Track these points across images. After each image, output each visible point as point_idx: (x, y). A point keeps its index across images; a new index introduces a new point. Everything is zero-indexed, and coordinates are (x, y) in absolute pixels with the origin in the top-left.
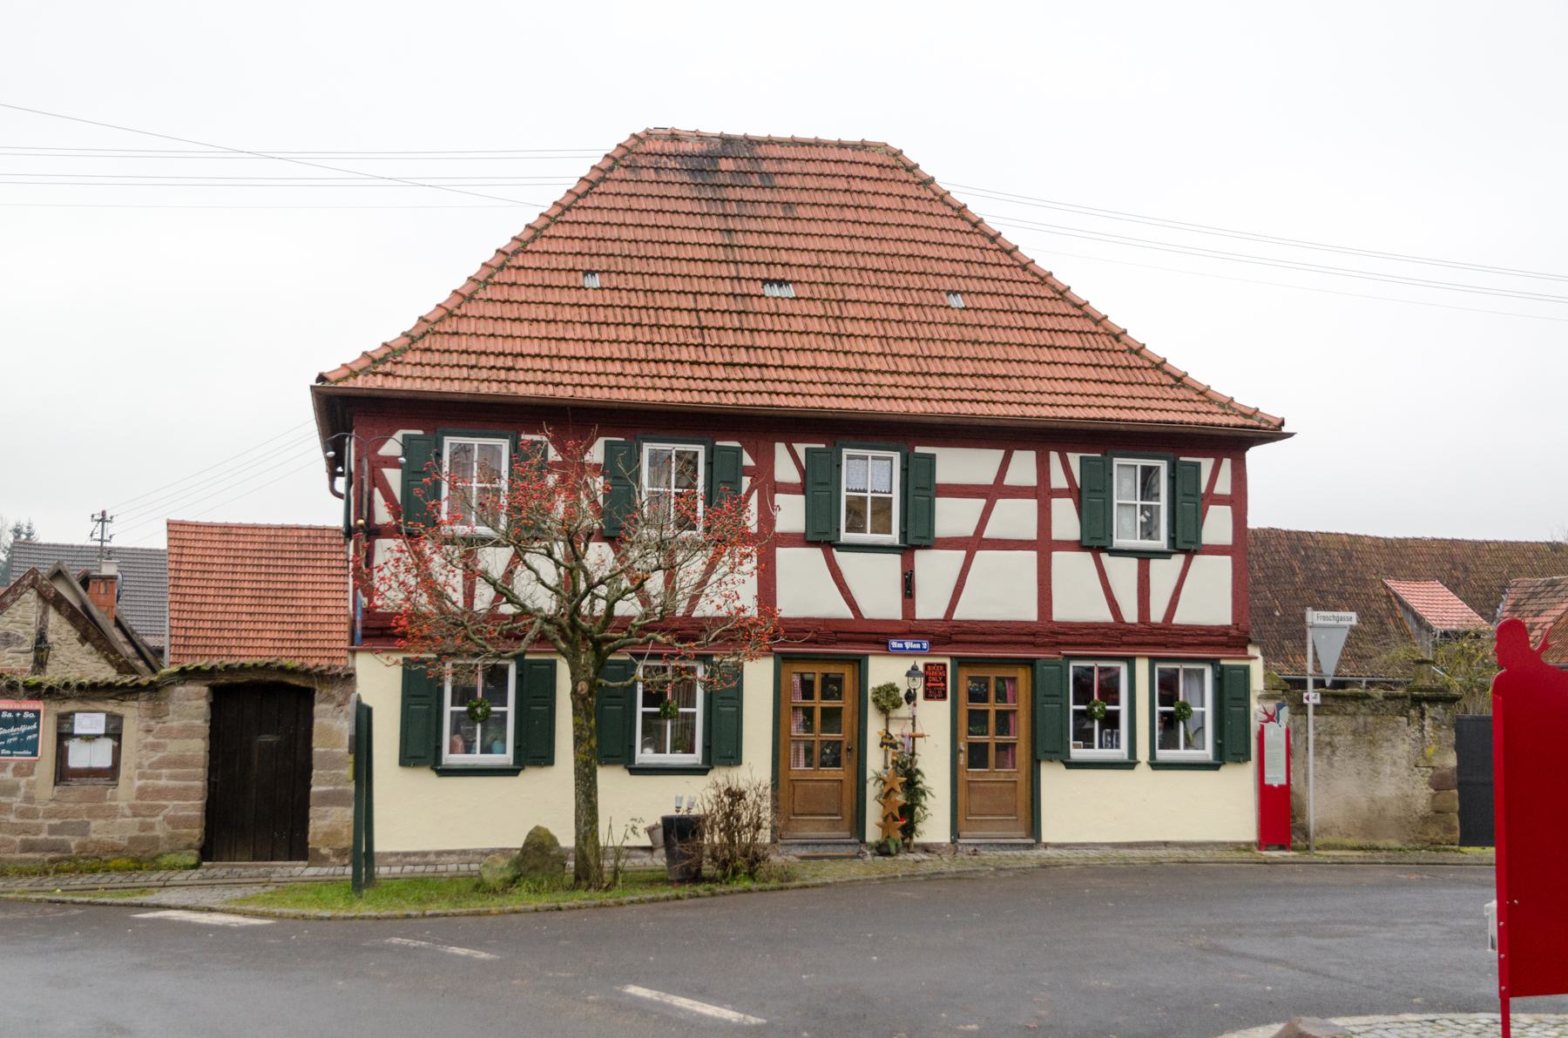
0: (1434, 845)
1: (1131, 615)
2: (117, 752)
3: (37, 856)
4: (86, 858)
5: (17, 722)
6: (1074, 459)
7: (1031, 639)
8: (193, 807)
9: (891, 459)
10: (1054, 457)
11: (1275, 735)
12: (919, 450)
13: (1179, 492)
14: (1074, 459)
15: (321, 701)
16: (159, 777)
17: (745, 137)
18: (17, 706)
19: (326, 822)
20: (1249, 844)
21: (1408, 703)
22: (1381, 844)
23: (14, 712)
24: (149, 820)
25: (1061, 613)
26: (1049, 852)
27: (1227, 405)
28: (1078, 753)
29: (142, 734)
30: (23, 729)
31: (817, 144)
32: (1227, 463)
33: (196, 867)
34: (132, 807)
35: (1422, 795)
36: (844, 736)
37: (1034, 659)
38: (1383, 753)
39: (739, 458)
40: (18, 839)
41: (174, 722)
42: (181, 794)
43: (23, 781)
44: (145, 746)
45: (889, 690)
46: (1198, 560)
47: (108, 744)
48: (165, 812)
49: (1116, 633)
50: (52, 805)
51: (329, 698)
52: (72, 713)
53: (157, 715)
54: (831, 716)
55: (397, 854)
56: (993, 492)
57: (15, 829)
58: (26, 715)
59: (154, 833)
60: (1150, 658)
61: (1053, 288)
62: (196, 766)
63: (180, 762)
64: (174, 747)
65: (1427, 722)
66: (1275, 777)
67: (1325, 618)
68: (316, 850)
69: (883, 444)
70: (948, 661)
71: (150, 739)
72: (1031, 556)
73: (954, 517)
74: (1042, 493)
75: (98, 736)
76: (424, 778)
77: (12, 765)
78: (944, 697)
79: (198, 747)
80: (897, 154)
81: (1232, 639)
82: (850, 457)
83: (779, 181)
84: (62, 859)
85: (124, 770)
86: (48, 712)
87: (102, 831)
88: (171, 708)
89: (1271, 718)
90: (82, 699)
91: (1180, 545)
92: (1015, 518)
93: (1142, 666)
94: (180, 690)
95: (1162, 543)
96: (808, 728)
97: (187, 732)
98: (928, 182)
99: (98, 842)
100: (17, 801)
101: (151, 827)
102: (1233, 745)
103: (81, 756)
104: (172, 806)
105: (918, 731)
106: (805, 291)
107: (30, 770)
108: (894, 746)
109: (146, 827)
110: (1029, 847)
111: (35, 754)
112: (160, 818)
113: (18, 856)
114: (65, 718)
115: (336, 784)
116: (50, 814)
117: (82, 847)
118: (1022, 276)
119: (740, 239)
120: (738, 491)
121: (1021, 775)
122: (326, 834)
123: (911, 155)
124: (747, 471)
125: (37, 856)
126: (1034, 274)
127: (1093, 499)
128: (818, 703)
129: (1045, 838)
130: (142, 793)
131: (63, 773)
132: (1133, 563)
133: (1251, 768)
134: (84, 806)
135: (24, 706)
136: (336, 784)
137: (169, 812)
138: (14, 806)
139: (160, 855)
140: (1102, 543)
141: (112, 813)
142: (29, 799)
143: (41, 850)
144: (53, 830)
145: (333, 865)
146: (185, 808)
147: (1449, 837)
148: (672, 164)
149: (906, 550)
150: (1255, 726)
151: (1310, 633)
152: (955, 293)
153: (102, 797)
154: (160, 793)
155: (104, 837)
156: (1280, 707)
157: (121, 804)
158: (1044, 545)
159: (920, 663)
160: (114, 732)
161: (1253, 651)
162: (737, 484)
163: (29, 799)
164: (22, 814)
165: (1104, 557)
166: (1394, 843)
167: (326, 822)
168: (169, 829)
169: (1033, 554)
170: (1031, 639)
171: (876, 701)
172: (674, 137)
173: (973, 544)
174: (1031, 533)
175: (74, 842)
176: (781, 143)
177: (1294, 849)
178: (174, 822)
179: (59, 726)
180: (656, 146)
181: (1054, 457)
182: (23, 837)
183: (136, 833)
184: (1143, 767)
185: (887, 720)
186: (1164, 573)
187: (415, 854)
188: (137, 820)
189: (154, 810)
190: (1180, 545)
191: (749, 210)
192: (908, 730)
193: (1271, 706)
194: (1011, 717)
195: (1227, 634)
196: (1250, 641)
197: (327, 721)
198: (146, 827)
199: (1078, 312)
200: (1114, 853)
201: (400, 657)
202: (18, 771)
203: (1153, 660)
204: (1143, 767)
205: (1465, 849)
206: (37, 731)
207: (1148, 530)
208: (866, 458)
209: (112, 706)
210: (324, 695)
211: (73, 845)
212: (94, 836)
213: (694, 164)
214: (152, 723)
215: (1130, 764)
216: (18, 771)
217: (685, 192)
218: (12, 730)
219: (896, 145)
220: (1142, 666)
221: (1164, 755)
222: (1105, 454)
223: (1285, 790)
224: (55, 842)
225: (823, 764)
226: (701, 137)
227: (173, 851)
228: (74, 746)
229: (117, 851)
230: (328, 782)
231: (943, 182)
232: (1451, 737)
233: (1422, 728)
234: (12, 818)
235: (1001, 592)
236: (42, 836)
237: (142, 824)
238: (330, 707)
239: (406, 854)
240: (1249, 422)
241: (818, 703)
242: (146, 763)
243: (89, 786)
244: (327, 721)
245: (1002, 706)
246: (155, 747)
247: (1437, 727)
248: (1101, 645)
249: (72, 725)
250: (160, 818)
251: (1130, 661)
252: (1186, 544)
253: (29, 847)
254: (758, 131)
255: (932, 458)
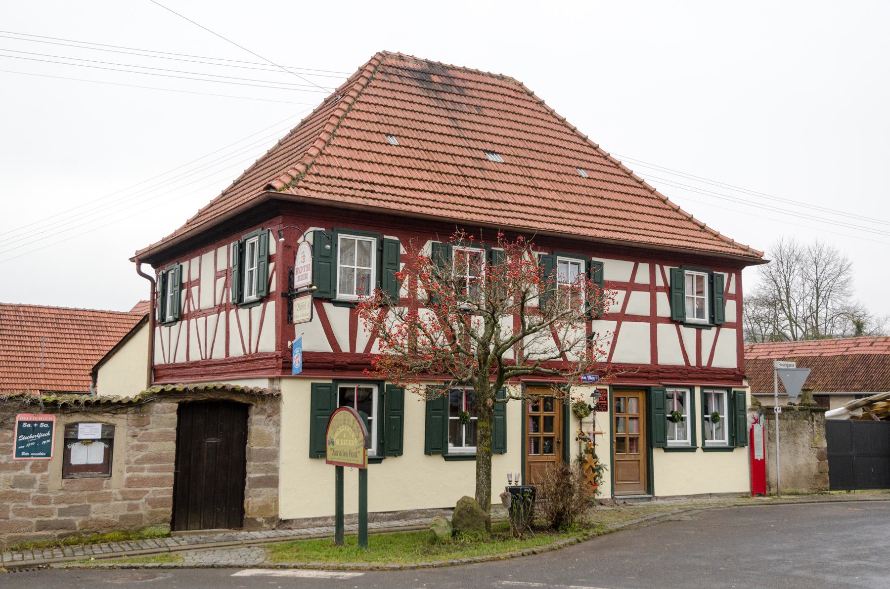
0: (820, 491)
1: (693, 362)
2: (109, 454)
3: (49, 533)
4: (87, 533)
5: (34, 430)
6: (667, 269)
7: (646, 375)
8: (166, 492)
9: (578, 264)
10: (657, 267)
11: (758, 430)
12: (594, 259)
13: (385, 262)
14: (667, 269)
15: (257, 414)
16: (142, 470)
17: (440, 64)
18: (35, 419)
19: (260, 499)
20: (747, 493)
21: (809, 412)
22: (799, 491)
23: (32, 423)
24: (134, 502)
25: (662, 360)
26: (659, 502)
27: (731, 243)
28: (452, 449)
29: (130, 439)
30: (39, 436)
31: (477, 73)
32: (734, 275)
33: (168, 535)
34: (122, 493)
35: (814, 461)
36: (555, 434)
37: (649, 387)
38: (799, 440)
39: (398, 249)
40: (34, 520)
41: (153, 429)
42: (158, 482)
43: (38, 476)
44: (132, 448)
45: (581, 405)
46: (722, 330)
47: (101, 447)
48: (146, 496)
49: (686, 372)
50: (61, 493)
51: (263, 411)
52: (77, 424)
53: (141, 424)
54: (549, 421)
55: (308, 519)
56: (630, 287)
57: (32, 513)
58: (42, 425)
59: (139, 512)
60: (701, 387)
61: (624, 170)
62: (170, 462)
63: (158, 458)
64: (154, 448)
65: (815, 423)
66: (759, 456)
67: (782, 365)
68: (254, 519)
69: (577, 254)
70: (607, 388)
71: (136, 442)
72: (647, 325)
73: (614, 302)
74: (652, 288)
75: (93, 440)
76: (437, 461)
77: (30, 463)
78: (606, 410)
79: (170, 447)
80: (521, 85)
81: (735, 376)
82: (560, 262)
83: (467, 92)
84: (68, 535)
85: (116, 466)
86: (59, 423)
87: (99, 512)
88: (151, 419)
89: (757, 421)
90: (85, 413)
91: (717, 322)
92: (639, 303)
93: (697, 391)
94: (158, 406)
95: (706, 320)
96: (536, 430)
97: (163, 437)
98: (541, 103)
99: (96, 520)
100: (34, 492)
101: (136, 507)
102: (739, 437)
103: (80, 456)
104: (152, 491)
105: (597, 430)
106: (508, 160)
107: (45, 468)
108: (585, 440)
109: (133, 507)
110: (649, 499)
111: (48, 455)
112: (143, 500)
113: (34, 533)
114: (71, 428)
115: (267, 472)
116: (59, 501)
117: (85, 524)
118: (605, 162)
119: (461, 124)
120: (398, 270)
121: (641, 456)
122: (260, 507)
123: (529, 86)
124: (403, 258)
125: (49, 533)
126: (612, 162)
127: (675, 292)
128: (542, 413)
129: (657, 493)
130: (130, 482)
131: (68, 469)
132: (346, 311)
133: (746, 450)
134: (86, 493)
135: (40, 419)
136: (267, 472)
137: (150, 495)
138: (32, 495)
139: (144, 528)
140: (680, 319)
141: (107, 498)
142: (43, 489)
143: (52, 529)
144: (62, 512)
145: (266, 529)
146: (162, 492)
147: (825, 486)
148: (406, 74)
149: (590, 318)
150: (749, 425)
151: (776, 372)
152: (391, 136)
153: (100, 486)
154: (143, 482)
155: (102, 516)
156: (760, 415)
157: (114, 491)
158: (653, 319)
159: (593, 389)
160: (108, 440)
161: (745, 383)
162: (397, 265)
163: (43, 489)
164: (38, 501)
165: (681, 327)
166: (805, 491)
167: (260, 499)
168: (150, 508)
169: (648, 325)
170: (646, 375)
171: (575, 412)
172: (401, 57)
173: (621, 317)
174: (647, 312)
175: (78, 521)
176: (459, 69)
177: (770, 495)
178: (152, 503)
179: (66, 433)
180: (389, 62)
181: (657, 267)
182: (39, 519)
183: (125, 513)
184: (699, 451)
185: (581, 423)
186: (708, 335)
187: (320, 519)
188: (125, 502)
189: (138, 495)
190: (717, 322)
191: (458, 107)
192: (591, 430)
193: (756, 414)
194: (257, 423)
195: (735, 374)
196: (745, 378)
197: (261, 428)
198: (133, 507)
199: (638, 185)
200: (689, 501)
201: (424, 386)
202: (34, 468)
203: (703, 388)
204: (699, 451)
205: (832, 492)
206: (50, 437)
207: (700, 313)
208: (566, 263)
209: (107, 418)
210: (258, 410)
211: (77, 523)
212: (93, 516)
213: (418, 76)
214: (137, 430)
215: (692, 449)
216: (34, 468)
217: (419, 92)
218: (31, 437)
219: (519, 79)
220: (697, 391)
221: (709, 443)
222: (681, 267)
223: (763, 461)
224: (63, 522)
225: (545, 452)
226: (416, 61)
227: (152, 525)
228: (75, 448)
229: (111, 526)
230: (262, 471)
231: (550, 104)
232: (823, 430)
233: (813, 427)
234: (30, 505)
235: (631, 347)
236: (54, 517)
237: (130, 505)
238: (263, 417)
239: (314, 519)
240: (746, 253)
241: (542, 413)
242: (133, 460)
243: (90, 478)
244: (261, 428)
245: (547, 414)
246: (139, 448)
247: (818, 426)
248: (678, 379)
249: (77, 432)
250: (143, 500)
251: (692, 388)
252: (717, 322)
253: (42, 526)
254: (446, 62)
255: (601, 264)
